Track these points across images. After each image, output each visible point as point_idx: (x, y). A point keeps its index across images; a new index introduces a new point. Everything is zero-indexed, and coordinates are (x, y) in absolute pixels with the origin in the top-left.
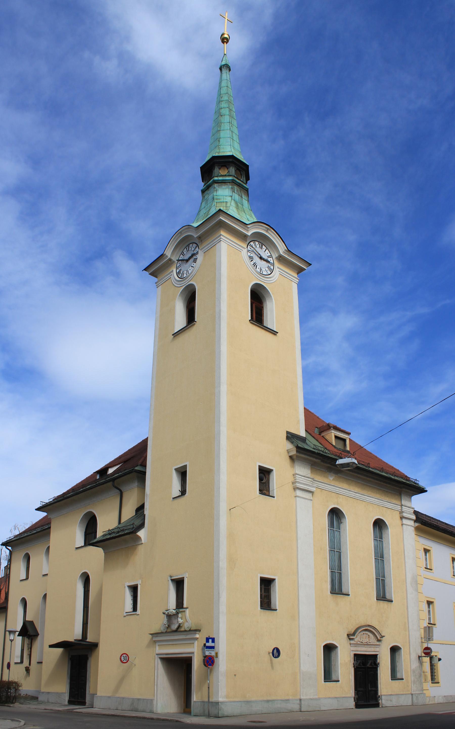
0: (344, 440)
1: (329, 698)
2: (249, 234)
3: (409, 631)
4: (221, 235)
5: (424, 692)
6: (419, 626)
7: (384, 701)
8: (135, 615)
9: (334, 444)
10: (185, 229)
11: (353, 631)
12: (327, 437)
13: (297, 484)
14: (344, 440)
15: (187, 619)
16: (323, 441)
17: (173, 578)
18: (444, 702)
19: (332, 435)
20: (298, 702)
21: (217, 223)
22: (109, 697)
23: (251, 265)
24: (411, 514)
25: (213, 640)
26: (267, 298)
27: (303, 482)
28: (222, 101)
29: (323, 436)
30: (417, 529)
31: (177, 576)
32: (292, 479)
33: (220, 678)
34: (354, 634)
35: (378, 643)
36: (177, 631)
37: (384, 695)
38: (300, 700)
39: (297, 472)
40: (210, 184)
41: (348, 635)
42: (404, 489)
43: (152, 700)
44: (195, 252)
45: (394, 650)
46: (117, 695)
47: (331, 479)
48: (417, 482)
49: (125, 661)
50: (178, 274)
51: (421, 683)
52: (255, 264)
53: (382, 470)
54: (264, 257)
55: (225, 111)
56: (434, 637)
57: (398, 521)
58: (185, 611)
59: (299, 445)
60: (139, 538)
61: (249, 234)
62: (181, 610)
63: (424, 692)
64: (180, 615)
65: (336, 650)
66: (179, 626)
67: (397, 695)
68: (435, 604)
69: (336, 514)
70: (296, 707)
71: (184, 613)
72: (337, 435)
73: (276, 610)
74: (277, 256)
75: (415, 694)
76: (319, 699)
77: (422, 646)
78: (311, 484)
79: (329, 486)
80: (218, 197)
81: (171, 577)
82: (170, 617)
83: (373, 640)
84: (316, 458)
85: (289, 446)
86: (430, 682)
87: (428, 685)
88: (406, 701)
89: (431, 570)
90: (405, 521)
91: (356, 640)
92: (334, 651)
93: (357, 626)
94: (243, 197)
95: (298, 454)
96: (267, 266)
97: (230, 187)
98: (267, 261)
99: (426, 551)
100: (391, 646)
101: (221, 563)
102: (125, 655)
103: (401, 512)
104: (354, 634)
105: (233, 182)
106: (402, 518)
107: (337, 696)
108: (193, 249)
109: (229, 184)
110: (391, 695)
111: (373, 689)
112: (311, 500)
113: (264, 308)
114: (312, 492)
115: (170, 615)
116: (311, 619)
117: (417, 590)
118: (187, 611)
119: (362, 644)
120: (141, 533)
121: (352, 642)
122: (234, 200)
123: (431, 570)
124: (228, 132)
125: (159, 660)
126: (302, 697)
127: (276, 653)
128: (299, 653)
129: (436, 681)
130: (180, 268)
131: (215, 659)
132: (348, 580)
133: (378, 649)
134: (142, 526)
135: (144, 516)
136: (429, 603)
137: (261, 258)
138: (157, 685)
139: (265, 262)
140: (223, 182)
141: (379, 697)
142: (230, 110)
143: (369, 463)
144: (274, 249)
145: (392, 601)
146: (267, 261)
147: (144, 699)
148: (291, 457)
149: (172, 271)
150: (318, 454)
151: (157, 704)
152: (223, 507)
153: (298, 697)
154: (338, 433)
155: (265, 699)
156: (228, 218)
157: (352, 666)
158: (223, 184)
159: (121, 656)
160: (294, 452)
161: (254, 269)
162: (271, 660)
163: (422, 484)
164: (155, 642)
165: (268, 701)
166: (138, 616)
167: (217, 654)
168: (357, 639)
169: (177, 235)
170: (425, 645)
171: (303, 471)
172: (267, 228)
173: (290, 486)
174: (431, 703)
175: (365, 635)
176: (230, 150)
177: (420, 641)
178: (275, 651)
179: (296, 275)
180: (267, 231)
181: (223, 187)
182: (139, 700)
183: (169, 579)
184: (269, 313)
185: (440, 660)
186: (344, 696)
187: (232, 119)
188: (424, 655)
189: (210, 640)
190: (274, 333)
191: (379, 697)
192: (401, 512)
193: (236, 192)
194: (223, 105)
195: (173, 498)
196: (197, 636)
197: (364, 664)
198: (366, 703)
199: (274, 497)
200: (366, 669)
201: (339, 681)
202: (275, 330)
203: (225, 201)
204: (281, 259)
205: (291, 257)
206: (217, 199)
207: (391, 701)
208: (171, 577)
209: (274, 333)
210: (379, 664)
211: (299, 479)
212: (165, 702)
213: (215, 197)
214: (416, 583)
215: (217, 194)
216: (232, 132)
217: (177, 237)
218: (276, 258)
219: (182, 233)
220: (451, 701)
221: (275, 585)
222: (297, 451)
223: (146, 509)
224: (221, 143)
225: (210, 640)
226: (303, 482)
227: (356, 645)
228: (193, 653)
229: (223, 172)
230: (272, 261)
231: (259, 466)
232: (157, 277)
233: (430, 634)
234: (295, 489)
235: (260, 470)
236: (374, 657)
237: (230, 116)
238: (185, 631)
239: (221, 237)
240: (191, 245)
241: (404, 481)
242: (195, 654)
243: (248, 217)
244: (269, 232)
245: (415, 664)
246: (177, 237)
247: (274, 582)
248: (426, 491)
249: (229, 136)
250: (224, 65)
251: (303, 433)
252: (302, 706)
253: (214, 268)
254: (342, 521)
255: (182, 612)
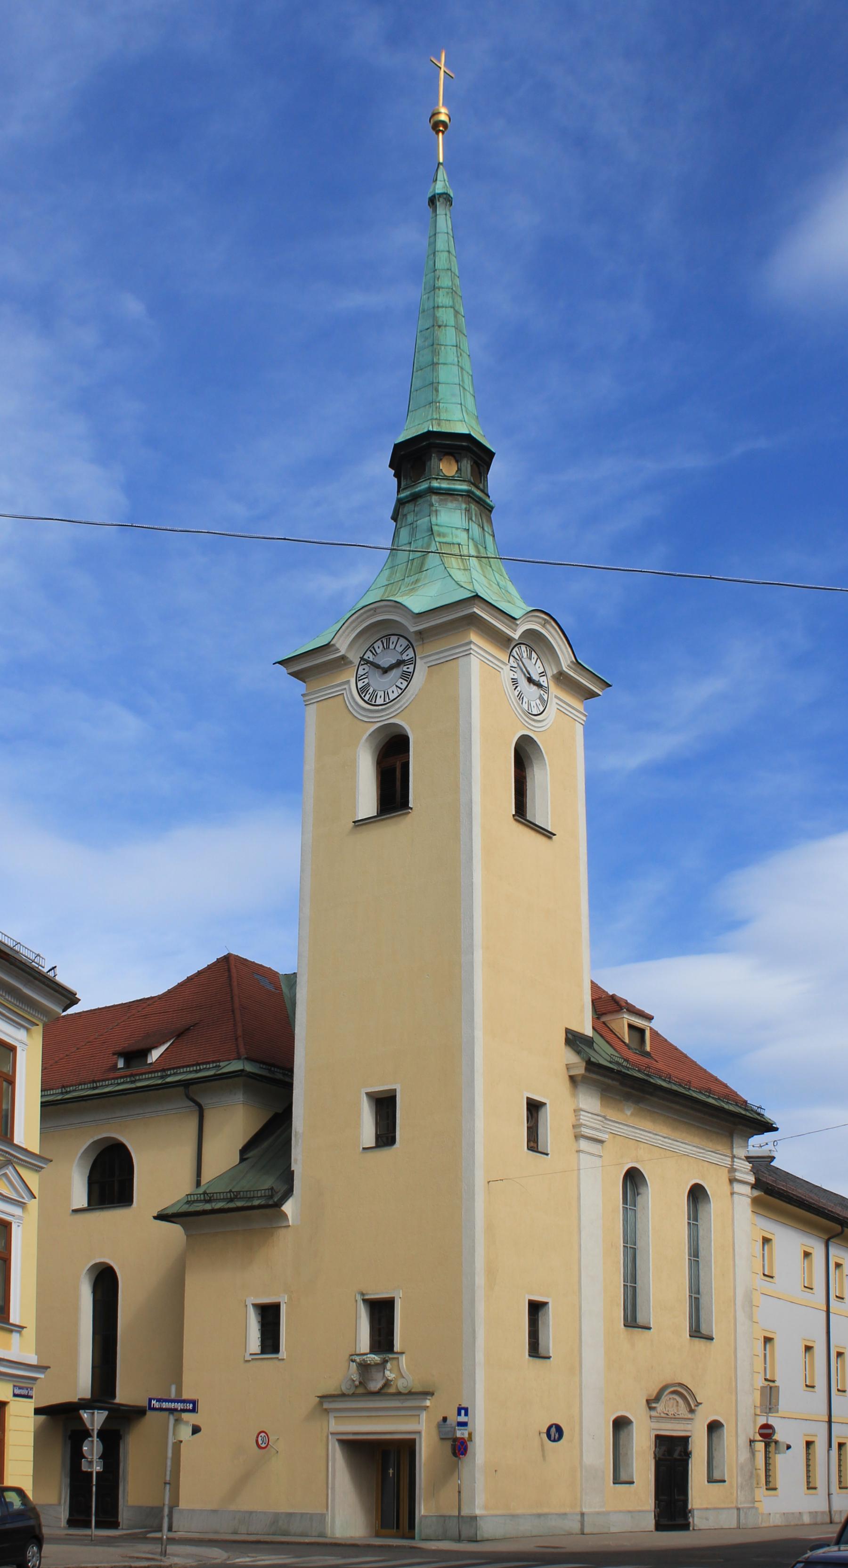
0: (642, 1032)
1: (621, 1512)
2: (516, 636)
3: (736, 1394)
4: (471, 642)
5: (757, 1505)
6: (752, 1385)
7: (697, 1520)
8: (276, 1361)
9: (627, 1041)
10: (386, 606)
11: (655, 1394)
12: (614, 1026)
13: (583, 1129)
14: (642, 1032)
15: (403, 1370)
16: (604, 1031)
17: (367, 1297)
18: (783, 1524)
19: (622, 1023)
20: (579, 1517)
21: (463, 617)
22: (214, 1511)
23: (514, 694)
24: (747, 1173)
25: (466, 1410)
26: (535, 762)
27: (590, 1123)
28: (439, 288)
29: (604, 1023)
30: (755, 1201)
31: (377, 1294)
32: (571, 1119)
33: (477, 1476)
34: (657, 1399)
35: (690, 1416)
36: (378, 1393)
37: (698, 1509)
38: (582, 1514)
39: (582, 1106)
40: (420, 491)
41: (648, 1402)
42: (740, 1127)
43: (323, 1516)
44: (405, 657)
45: (714, 1427)
46: (233, 1507)
47: (629, 1113)
48: (762, 1112)
49: (263, 1445)
50: (362, 691)
51: (752, 1491)
52: (520, 696)
53: (709, 1092)
54: (535, 677)
55: (446, 316)
56: (780, 1407)
57: (726, 1187)
58: (398, 1358)
59: (592, 1059)
60: (284, 1216)
61: (516, 636)
62: (391, 1356)
63: (757, 1505)
64: (389, 1365)
65: (630, 1427)
66: (387, 1384)
67: (715, 1509)
68: (777, 1342)
69: (633, 1179)
70: (576, 1527)
71: (395, 1362)
72: (631, 1022)
73: (549, 1358)
74: (555, 672)
75: (743, 1508)
76: (607, 1513)
77: (755, 1422)
78: (600, 1127)
79: (625, 1128)
80: (442, 530)
81: (363, 1294)
82: (365, 1368)
83: (683, 1411)
84: (613, 1079)
85: (572, 1058)
86: (765, 1487)
87: (761, 1492)
88: (728, 1520)
89: (772, 1277)
90: (738, 1188)
91: (659, 1409)
92: (625, 1430)
93: (661, 1386)
94: (486, 528)
95: (587, 1074)
96: (538, 696)
97: (464, 506)
98: (539, 685)
99: (766, 1241)
100: (709, 1421)
101: (477, 1279)
102: (263, 1434)
103: (732, 1170)
104: (657, 1399)
105: (469, 496)
106: (732, 1181)
107: (630, 1509)
108: (399, 649)
109: (460, 499)
110: (707, 1509)
111: (682, 1497)
112: (601, 1156)
113: (528, 780)
114: (601, 1142)
115: (369, 1365)
116: (600, 1375)
117: (751, 1317)
118: (403, 1359)
119: (667, 1418)
120: (288, 1207)
121: (653, 1413)
122: (473, 539)
123: (772, 1277)
124: (455, 369)
125: (337, 1444)
126: (584, 1510)
127: (555, 1433)
128: (581, 1434)
129: (771, 1485)
130: (366, 681)
131: (468, 1443)
132: (649, 1301)
133: (689, 1427)
134: (289, 1192)
135: (291, 1174)
136: (768, 1340)
137: (530, 680)
138: (333, 1488)
139: (535, 688)
140: (449, 494)
141: (690, 1511)
142: (457, 312)
143: (689, 1082)
144: (551, 660)
145: (711, 1339)
146: (539, 685)
147: (302, 1514)
148: (572, 1079)
149: (348, 682)
150: (619, 1072)
151: (333, 1518)
152: (480, 1178)
153: (578, 1510)
154: (633, 1019)
155: (535, 1511)
156: (487, 608)
157: (653, 1456)
158: (450, 498)
159: (257, 1437)
160: (580, 1070)
161: (518, 704)
162: (542, 1445)
163: (770, 1115)
164: (327, 1411)
165: (539, 1515)
166: (281, 1362)
167: (470, 1434)
168: (660, 1407)
169: (365, 612)
170: (762, 1421)
171: (589, 1103)
172: (545, 620)
173: (571, 1133)
174: (764, 1525)
175: (672, 1401)
176: (460, 417)
177: (752, 1412)
178: (553, 1430)
179: (580, 707)
180: (544, 626)
181: (450, 505)
182: (290, 1515)
183: (359, 1298)
184: (538, 792)
185: (789, 1447)
186: (640, 1508)
187: (461, 336)
188: (761, 1439)
189: (463, 1412)
190: (549, 835)
191: (690, 1511)
192: (732, 1170)
193: (474, 519)
194: (443, 299)
195: (364, 1149)
196: (428, 1403)
197: (670, 1452)
198: (670, 1523)
199: (547, 1154)
200: (672, 1458)
201: (632, 1483)
202: (550, 830)
203: (456, 540)
204: (561, 678)
205: (580, 675)
206: (439, 535)
207: (707, 1519)
208: (363, 1294)
209: (549, 835)
210: (691, 1453)
211: (584, 1118)
212: (346, 1514)
213: (435, 528)
214: (750, 1304)
215: (439, 522)
216: (462, 368)
217: (365, 616)
218: (553, 676)
219: (378, 611)
220: (792, 1523)
221: (547, 1314)
222: (586, 1069)
223: (296, 1160)
224: (441, 396)
225: (463, 1412)
226: (590, 1123)
227: (659, 1419)
228: (419, 1433)
229: (448, 468)
230: (545, 684)
231: (528, 1098)
232: (305, 682)
233: (773, 1401)
234: (578, 1137)
235: (528, 1104)
236: (684, 1441)
237: (456, 329)
238: (399, 1394)
239: (472, 646)
240: (394, 639)
241: (743, 1112)
242: (423, 1434)
243: (518, 608)
244: (548, 626)
245: (744, 1455)
246: (365, 616)
247: (546, 1307)
248: (776, 1129)
249: (456, 380)
250: (440, 195)
251: (588, 1031)
252: (586, 1524)
253: (454, 706)
254: (641, 1191)
255: (393, 1358)
